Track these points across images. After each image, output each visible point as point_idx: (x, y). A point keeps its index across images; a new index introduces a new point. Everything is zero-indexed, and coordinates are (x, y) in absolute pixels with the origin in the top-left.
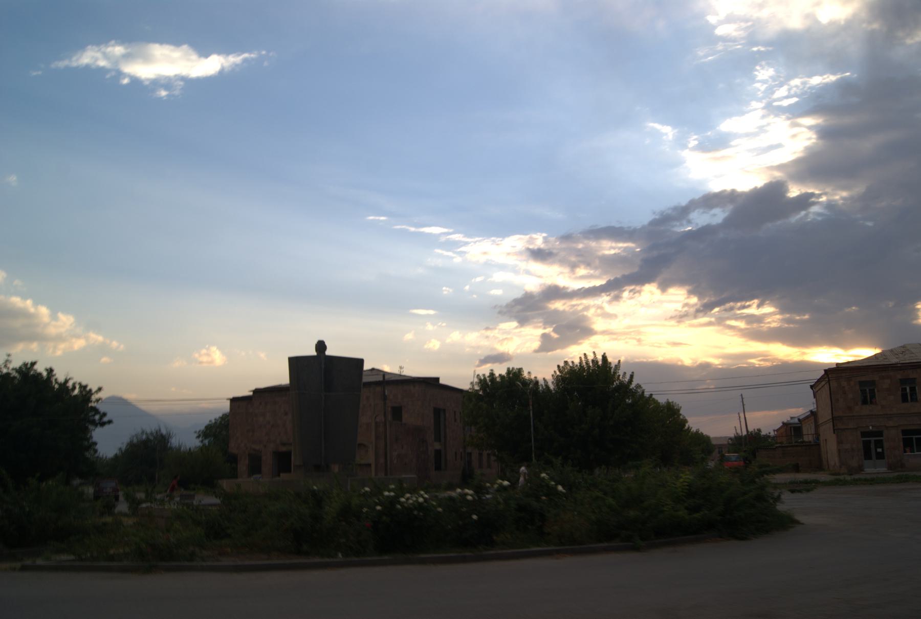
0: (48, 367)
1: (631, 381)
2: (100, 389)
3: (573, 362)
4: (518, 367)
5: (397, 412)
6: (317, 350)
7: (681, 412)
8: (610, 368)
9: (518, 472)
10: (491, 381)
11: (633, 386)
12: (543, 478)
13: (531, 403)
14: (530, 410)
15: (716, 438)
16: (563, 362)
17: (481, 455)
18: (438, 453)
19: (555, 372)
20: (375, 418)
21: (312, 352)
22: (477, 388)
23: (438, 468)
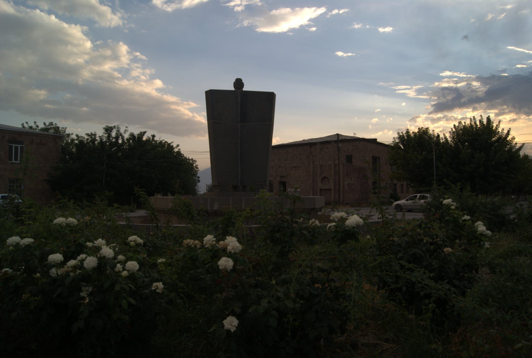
0: (152, 134)
2: (178, 146)
5: (349, 158)
9: (312, 219)
11: (509, 138)
12: (448, 206)
14: (433, 155)
17: (402, 185)
19: (452, 129)
20: (334, 161)
22: (397, 141)
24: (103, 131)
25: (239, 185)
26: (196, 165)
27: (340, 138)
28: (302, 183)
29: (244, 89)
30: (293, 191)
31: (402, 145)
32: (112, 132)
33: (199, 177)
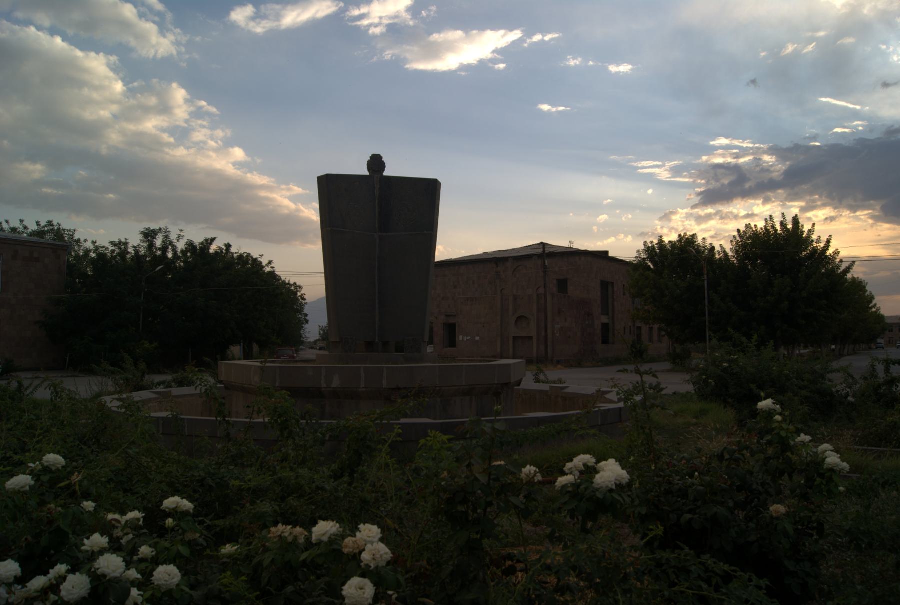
2: (270, 262)
3: (756, 226)
5: (563, 285)
6: (369, 171)
7: (867, 288)
8: (803, 232)
10: (660, 248)
11: (830, 252)
14: (704, 280)
15: (888, 317)
16: (744, 226)
17: (651, 329)
18: (605, 327)
21: (362, 170)
22: (643, 256)
23: (605, 341)
24: (141, 237)
25: (377, 341)
26: (302, 295)
27: (547, 251)
28: (484, 327)
29: (386, 174)
32: (156, 239)
33: (306, 315)
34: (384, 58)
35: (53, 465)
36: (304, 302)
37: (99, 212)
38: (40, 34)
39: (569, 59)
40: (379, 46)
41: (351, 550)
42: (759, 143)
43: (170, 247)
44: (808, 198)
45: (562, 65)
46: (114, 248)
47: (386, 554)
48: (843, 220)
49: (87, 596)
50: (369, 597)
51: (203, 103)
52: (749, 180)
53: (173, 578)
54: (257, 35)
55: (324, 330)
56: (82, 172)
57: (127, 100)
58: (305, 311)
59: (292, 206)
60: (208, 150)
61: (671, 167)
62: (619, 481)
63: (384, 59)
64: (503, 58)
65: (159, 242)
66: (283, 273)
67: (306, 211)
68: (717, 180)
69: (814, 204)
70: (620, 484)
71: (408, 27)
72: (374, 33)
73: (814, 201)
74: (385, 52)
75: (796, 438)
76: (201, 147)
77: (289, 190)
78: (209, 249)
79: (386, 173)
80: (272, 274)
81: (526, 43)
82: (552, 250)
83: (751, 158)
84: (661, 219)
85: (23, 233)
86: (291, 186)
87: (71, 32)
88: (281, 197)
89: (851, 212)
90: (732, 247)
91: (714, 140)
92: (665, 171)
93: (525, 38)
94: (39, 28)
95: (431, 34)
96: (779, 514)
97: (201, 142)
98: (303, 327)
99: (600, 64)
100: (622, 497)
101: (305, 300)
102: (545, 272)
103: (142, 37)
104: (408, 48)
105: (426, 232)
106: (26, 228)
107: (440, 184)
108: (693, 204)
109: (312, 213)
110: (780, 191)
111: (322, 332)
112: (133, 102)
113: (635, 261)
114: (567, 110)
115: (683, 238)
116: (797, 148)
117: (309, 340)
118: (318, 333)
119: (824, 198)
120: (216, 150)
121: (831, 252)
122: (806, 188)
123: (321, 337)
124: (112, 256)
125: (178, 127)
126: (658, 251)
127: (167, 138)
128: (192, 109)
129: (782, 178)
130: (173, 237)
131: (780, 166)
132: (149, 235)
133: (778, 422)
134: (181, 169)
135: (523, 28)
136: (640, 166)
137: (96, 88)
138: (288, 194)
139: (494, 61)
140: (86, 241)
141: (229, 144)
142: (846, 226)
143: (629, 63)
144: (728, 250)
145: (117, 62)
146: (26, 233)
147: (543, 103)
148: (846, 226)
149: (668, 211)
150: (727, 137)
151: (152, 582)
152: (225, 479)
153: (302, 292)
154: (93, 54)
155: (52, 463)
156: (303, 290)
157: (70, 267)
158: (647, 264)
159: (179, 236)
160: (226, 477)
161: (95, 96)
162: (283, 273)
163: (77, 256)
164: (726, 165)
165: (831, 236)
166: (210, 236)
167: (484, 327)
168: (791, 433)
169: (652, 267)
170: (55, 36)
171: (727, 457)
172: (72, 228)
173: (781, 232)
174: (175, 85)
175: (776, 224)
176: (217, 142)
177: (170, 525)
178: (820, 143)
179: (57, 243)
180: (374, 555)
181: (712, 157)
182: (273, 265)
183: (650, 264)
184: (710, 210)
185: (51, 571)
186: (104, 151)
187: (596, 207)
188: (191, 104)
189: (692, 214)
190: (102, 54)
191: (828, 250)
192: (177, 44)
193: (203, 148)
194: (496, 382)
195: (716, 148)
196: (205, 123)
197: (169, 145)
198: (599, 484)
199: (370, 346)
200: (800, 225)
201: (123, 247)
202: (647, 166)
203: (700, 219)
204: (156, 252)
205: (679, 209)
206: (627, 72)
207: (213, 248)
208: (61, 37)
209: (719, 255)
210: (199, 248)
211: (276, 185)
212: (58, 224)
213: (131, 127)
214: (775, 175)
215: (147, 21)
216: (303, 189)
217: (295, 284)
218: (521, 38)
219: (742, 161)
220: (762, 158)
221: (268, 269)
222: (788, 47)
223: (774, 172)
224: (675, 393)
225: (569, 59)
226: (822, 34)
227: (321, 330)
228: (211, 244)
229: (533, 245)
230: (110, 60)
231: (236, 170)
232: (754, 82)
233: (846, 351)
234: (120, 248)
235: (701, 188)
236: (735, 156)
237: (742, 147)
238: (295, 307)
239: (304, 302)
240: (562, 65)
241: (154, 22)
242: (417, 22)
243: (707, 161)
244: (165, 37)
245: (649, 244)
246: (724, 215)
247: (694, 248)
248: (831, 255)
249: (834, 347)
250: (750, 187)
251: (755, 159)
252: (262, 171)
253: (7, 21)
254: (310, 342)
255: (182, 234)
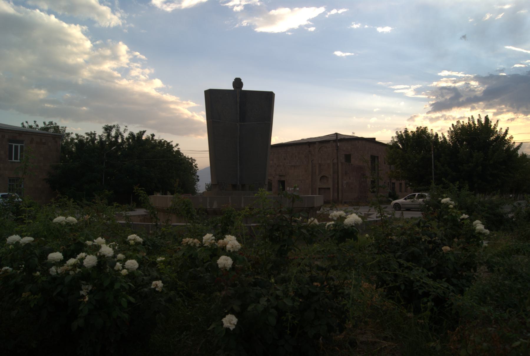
0: (152, 134)
1: (506, 133)
2: (177, 145)
4: (424, 127)
5: (348, 158)
6: (234, 87)
8: (491, 126)
11: (507, 137)
13: (432, 149)
14: (432, 154)
17: (401, 184)
19: (450, 128)
20: (333, 160)
22: (396, 140)
24: (103, 130)
25: (238, 184)
26: (195, 164)
27: (339, 138)
28: (301, 182)
29: (243, 89)
30: (292, 190)
31: (401, 144)
32: (112, 131)
33: (198, 176)
34: (243, 24)
35: (71, 222)
36: (196, 169)
37: (78, 118)
38: (42, 13)
39: (353, 24)
40: (240, 18)
41: (222, 245)
42: (468, 74)
43: (120, 136)
44: (498, 107)
45: (349, 28)
46: (88, 136)
47: (239, 245)
48: (519, 120)
49: (96, 265)
50: (230, 264)
51: (137, 53)
52: (462, 96)
53: (135, 266)
54: (167, 12)
55: (208, 186)
56: (67, 95)
57: (93, 52)
58: (198, 174)
59: (190, 114)
60: (140, 80)
61: (415, 88)
62: (357, 222)
63: (242, 26)
64: (313, 24)
65: (113, 133)
66: (184, 151)
67: (198, 116)
68: (443, 97)
69: (502, 111)
70: (357, 224)
71: (257, 6)
72: (236, 10)
73: (502, 109)
74: (243, 21)
75: (461, 217)
76: (136, 79)
77: (188, 104)
78: (142, 137)
79: (244, 88)
80: (178, 152)
81: (327, 15)
82: (342, 137)
83: (463, 83)
84: (408, 120)
85: (36, 128)
86: (189, 102)
87: (60, 13)
88: (183, 108)
89: (524, 115)
90: (448, 135)
91: (440, 72)
92: (411, 91)
93: (327, 12)
94: (41, 11)
95: (270, 10)
96: (447, 251)
97: (136, 76)
98: (196, 184)
99: (372, 27)
100: (358, 229)
101: (197, 167)
102: (337, 150)
103: (101, 14)
104: (257, 18)
105: (266, 122)
106: (37, 126)
107: (274, 94)
108: (427, 111)
109: (201, 118)
110: (481, 103)
111: (207, 187)
112: (96, 53)
113: (391, 143)
114: (352, 55)
115: (419, 129)
116: (491, 77)
117: (200, 192)
118: (205, 187)
119: (508, 107)
120: (145, 81)
121: (508, 138)
122: (497, 101)
123: (207, 190)
124: (87, 141)
125: (123, 67)
126: (405, 137)
127: (116, 74)
128: (131, 57)
129: (482, 95)
130: (122, 130)
131: (481, 88)
132: (108, 129)
133: (451, 208)
134: (124, 92)
135: (326, 6)
136: (396, 88)
137: (75, 45)
138: (187, 106)
139: (308, 26)
140: (72, 133)
141: (152, 77)
142: (521, 124)
143: (390, 26)
144: (446, 136)
145: (87, 30)
146: (38, 129)
147: (337, 51)
148: (521, 124)
149: (413, 115)
150: (449, 70)
151: (125, 267)
152: (156, 243)
153: (196, 163)
154: (73, 25)
155: (71, 221)
156: (196, 161)
157: (63, 147)
158: (398, 144)
159: (125, 130)
160: (157, 242)
161: (75, 50)
162: (184, 151)
163: (67, 142)
164: (448, 88)
165: (508, 128)
166: (142, 130)
167: (301, 182)
168: (458, 214)
169: (401, 146)
170: (51, 15)
171: (422, 225)
172: (64, 126)
173: (478, 125)
174: (120, 43)
175: (475, 121)
176: (145, 76)
177: (132, 244)
178: (505, 73)
179: (55, 134)
180: (232, 246)
181: (439, 82)
182: (178, 147)
183: (400, 145)
184: (438, 114)
185: (78, 256)
186: (80, 82)
187: (368, 112)
188: (130, 54)
189: (427, 117)
190: (78, 25)
191: (506, 136)
192: (122, 18)
193: (137, 80)
194: (306, 207)
195: (442, 77)
196: (139, 65)
197: (118, 78)
198: (346, 223)
199: (234, 187)
200: (489, 121)
201: (93, 136)
202: (399, 88)
203: (432, 120)
204: (112, 139)
205: (419, 114)
206: (388, 32)
207: (144, 138)
208: (54, 15)
209: (441, 139)
210: (136, 137)
211: (180, 101)
212: (55, 123)
213: (96, 68)
214: (478, 93)
215: (104, 5)
216: (196, 103)
217: (191, 158)
218: (324, 12)
219: (457, 85)
220: (470, 83)
221: (175, 149)
222: (487, 16)
223: (477, 91)
224: (412, 218)
225: (353, 24)
226: (507, 7)
227: (207, 185)
228: (143, 134)
229: (331, 134)
230: (83, 28)
231: (156, 93)
232: (464, 37)
233: (518, 198)
234: (91, 137)
235: (432, 101)
236: (453, 82)
237: (458, 76)
238: (192, 172)
239: (196, 169)
240: (349, 28)
241: (108, 6)
242: (262, 3)
243: (436, 85)
244: (114, 14)
245: (399, 133)
246: (447, 118)
247: (426, 135)
248: (508, 139)
249: (511, 196)
250: (463, 101)
251: (466, 83)
252: (172, 93)
253: (23, 6)
254: (200, 193)
255: (126, 128)
